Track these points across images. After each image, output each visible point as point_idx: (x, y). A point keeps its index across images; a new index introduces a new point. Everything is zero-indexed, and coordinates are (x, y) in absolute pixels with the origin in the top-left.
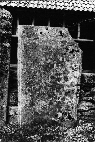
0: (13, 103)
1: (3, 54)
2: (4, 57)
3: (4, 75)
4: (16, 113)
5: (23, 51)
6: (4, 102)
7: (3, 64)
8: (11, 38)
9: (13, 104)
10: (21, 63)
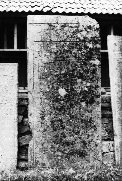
0: (106, 137)
1: (92, 75)
2: (93, 78)
3: (95, 101)
4: (109, 150)
5: (116, 69)
6: (98, 136)
7: (93, 87)
8: (101, 53)
9: (106, 138)
10: (115, 85)
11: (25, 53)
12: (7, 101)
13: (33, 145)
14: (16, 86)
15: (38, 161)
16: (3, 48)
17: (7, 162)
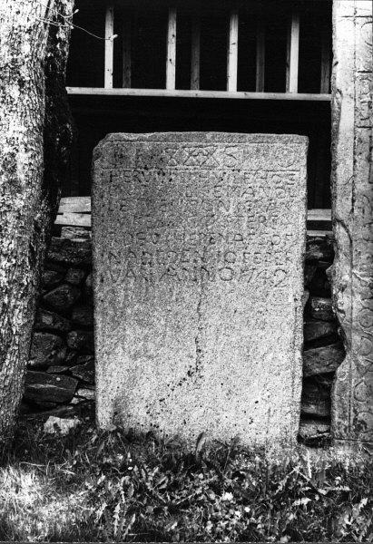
11: (327, 106)
12: (276, 247)
13: (350, 376)
14: (303, 205)
15: (362, 422)
16: (253, 90)
17: (272, 420)
